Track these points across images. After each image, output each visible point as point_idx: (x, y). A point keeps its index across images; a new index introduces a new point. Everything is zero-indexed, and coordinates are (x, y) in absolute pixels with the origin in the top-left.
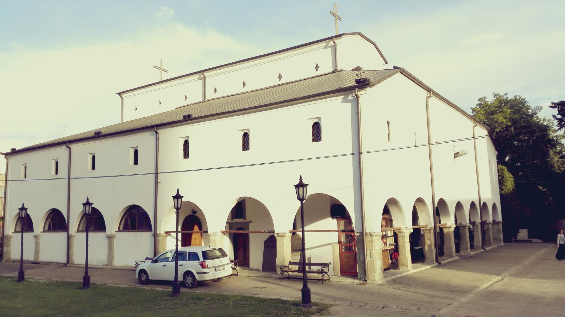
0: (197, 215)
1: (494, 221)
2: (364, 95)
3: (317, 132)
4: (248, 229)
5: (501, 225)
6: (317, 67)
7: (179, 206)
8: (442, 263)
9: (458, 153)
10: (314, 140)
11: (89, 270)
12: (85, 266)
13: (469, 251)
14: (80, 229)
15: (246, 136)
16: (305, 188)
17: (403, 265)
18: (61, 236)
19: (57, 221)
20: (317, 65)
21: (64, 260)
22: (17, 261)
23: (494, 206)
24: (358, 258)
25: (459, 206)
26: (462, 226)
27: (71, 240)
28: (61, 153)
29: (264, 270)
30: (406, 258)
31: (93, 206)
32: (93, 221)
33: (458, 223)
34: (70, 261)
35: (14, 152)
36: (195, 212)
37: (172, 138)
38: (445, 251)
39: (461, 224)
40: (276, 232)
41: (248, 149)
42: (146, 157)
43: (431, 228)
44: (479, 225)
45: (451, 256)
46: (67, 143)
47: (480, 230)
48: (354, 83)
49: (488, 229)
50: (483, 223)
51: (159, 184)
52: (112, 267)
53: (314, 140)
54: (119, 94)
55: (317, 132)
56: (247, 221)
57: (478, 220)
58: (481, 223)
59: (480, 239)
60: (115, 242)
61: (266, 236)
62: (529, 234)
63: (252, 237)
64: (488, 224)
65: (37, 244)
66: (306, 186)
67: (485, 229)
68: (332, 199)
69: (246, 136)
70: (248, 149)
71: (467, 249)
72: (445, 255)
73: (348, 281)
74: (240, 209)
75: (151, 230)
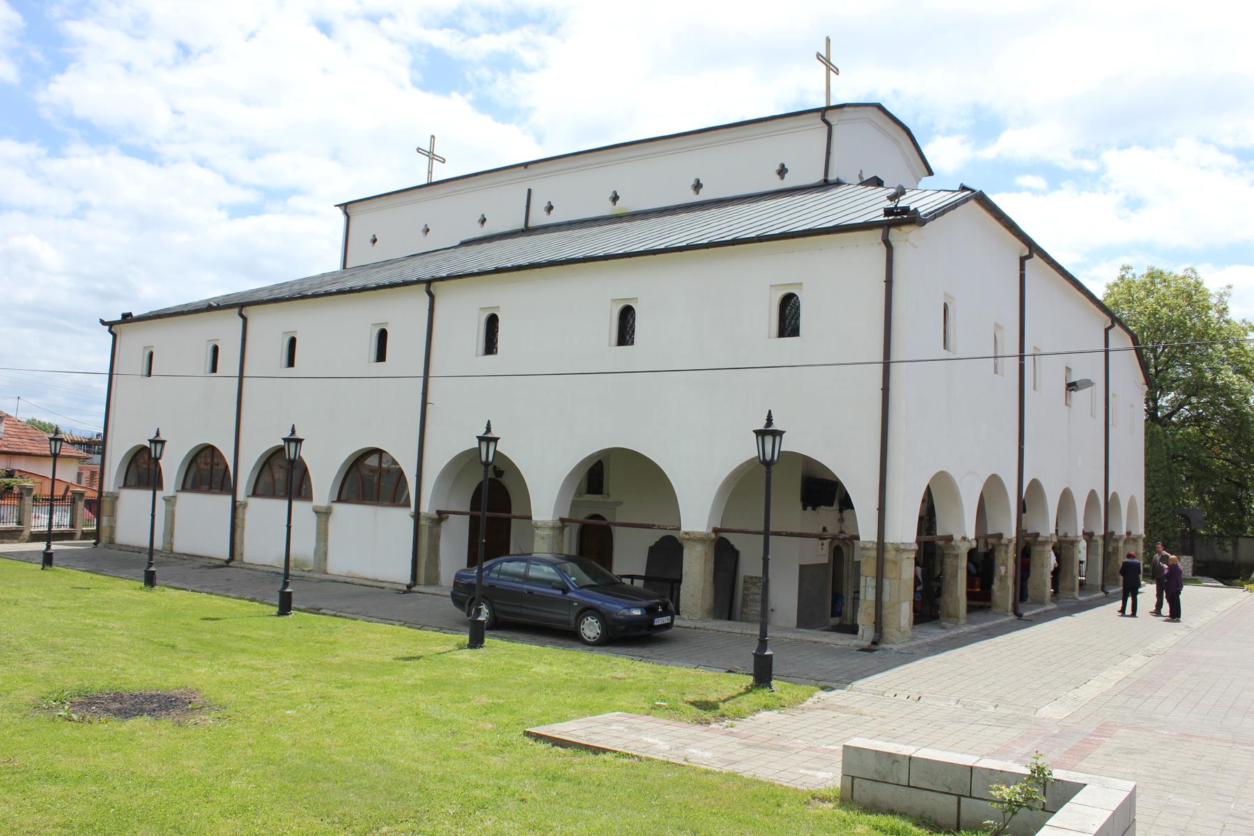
0: (505, 480)
1: (1129, 533)
2: (903, 238)
3: (789, 318)
4: (510, 512)
5: (1141, 544)
6: (615, 198)
7: (490, 459)
8: (1026, 614)
9: (1074, 384)
10: (782, 333)
11: (890, 555)
12: (282, 571)
13: (1076, 594)
14: (260, 489)
15: (383, 336)
16: (778, 439)
17: (949, 616)
18: (223, 502)
19: (207, 471)
20: (783, 166)
21: (226, 556)
22: (139, 550)
23: (1132, 502)
24: (862, 596)
25: (1066, 498)
26: (1067, 542)
27: (240, 511)
28: (226, 329)
29: (798, 626)
30: (957, 600)
31: (501, 447)
32: (284, 474)
33: (1060, 534)
34: (237, 557)
35: (127, 318)
36: (499, 473)
37: (269, 330)
38: (1031, 592)
39: (1066, 536)
40: (684, 529)
41: (795, 332)
42: (228, 362)
43: (1010, 541)
44: (1101, 542)
45: (1041, 603)
46: (241, 305)
47: (1100, 551)
48: (119, 318)
49: (1116, 550)
50: (1108, 536)
51: (429, 407)
52: (326, 577)
53: (782, 333)
54: (345, 207)
55: (789, 318)
56: (611, 500)
57: (1100, 531)
58: (1104, 537)
59: (1100, 569)
60: (333, 525)
61: (653, 537)
62: (1194, 567)
63: (619, 535)
64: (1117, 540)
65: (322, 536)
66: (781, 433)
67: (1110, 549)
68: (807, 461)
69: (383, 336)
70: (795, 332)
71: (1073, 590)
72: (1029, 600)
73: (724, 625)
74: (596, 475)
75: (407, 505)
